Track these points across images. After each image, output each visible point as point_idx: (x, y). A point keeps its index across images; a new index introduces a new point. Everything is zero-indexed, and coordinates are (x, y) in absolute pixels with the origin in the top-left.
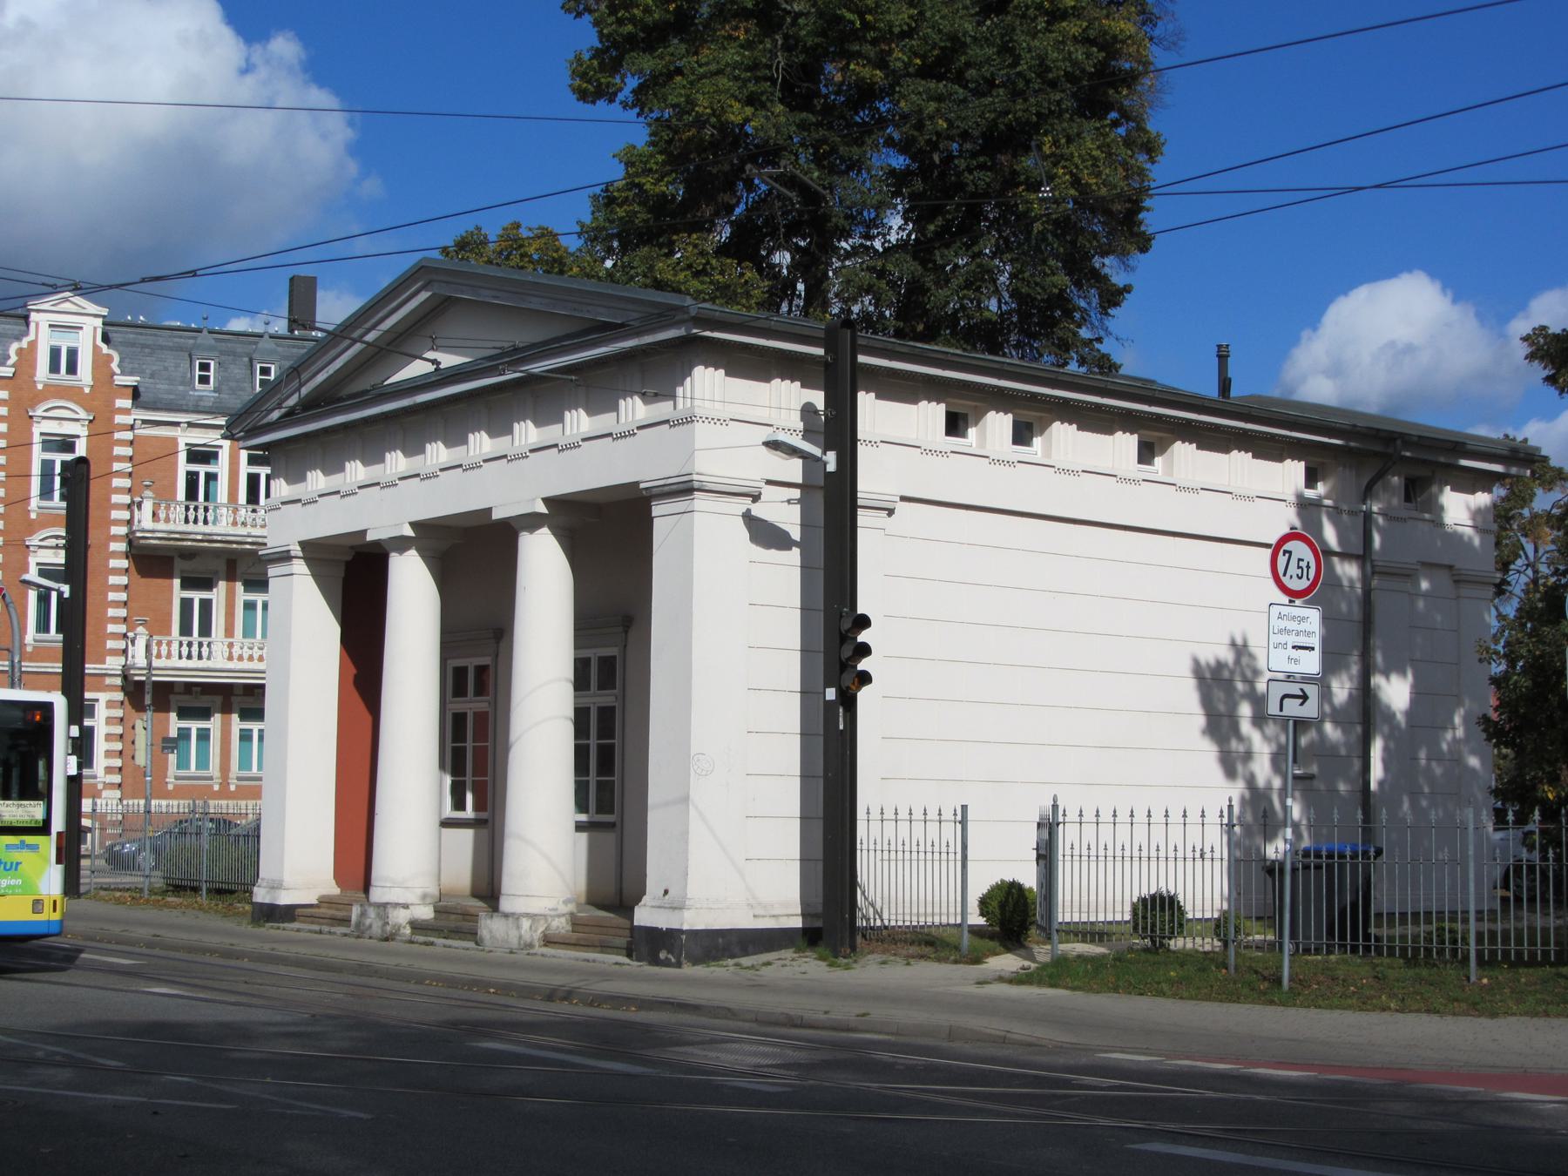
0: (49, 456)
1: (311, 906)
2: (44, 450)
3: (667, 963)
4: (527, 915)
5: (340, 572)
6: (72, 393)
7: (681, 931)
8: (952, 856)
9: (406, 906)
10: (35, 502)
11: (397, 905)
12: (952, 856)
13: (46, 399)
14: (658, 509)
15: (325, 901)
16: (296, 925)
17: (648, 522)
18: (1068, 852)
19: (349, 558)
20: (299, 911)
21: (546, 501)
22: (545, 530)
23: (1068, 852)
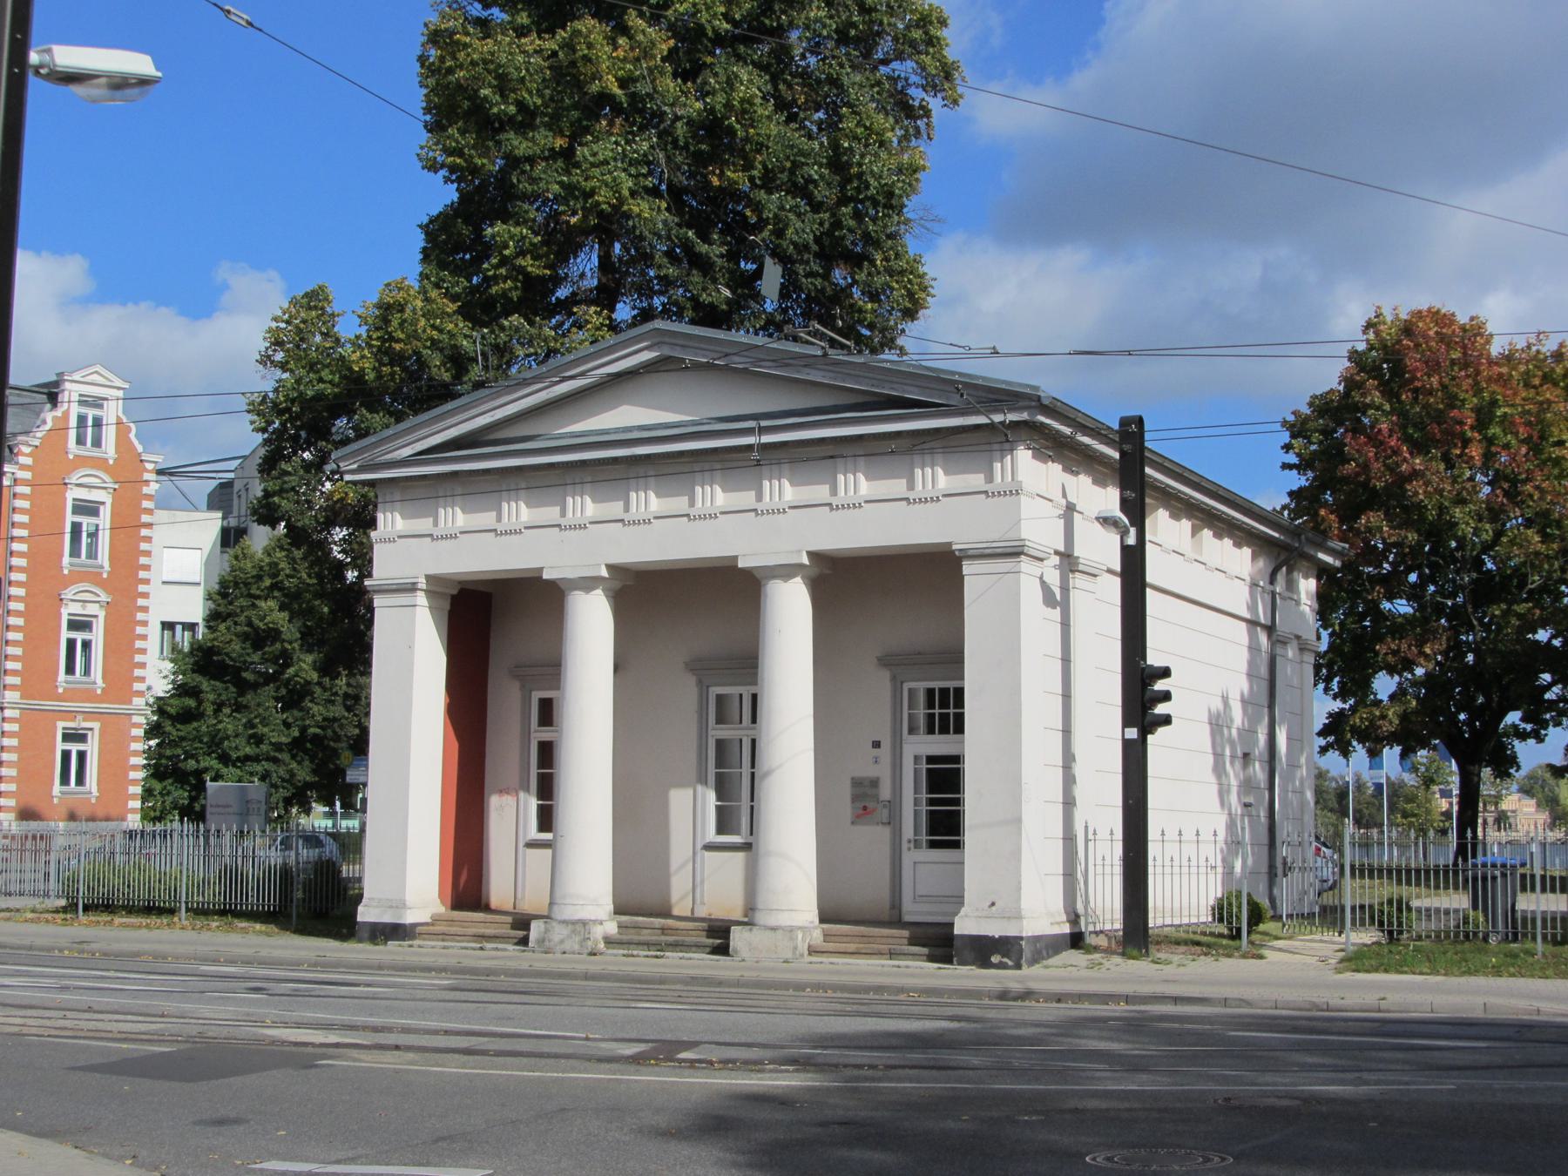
0: (78, 519)
1: (426, 924)
2: (74, 513)
3: (1002, 966)
4: (800, 928)
5: (447, 606)
6: (101, 463)
7: (1021, 938)
8: (1108, 870)
9: (601, 923)
10: (66, 559)
11: (594, 921)
12: (1108, 870)
13: (76, 468)
14: (968, 568)
15: (436, 920)
16: (416, 942)
17: (960, 579)
18: (1099, 861)
19: (455, 592)
20: (419, 929)
21: (810, 554)
22: (798, 579)
23: (1099, 861)
